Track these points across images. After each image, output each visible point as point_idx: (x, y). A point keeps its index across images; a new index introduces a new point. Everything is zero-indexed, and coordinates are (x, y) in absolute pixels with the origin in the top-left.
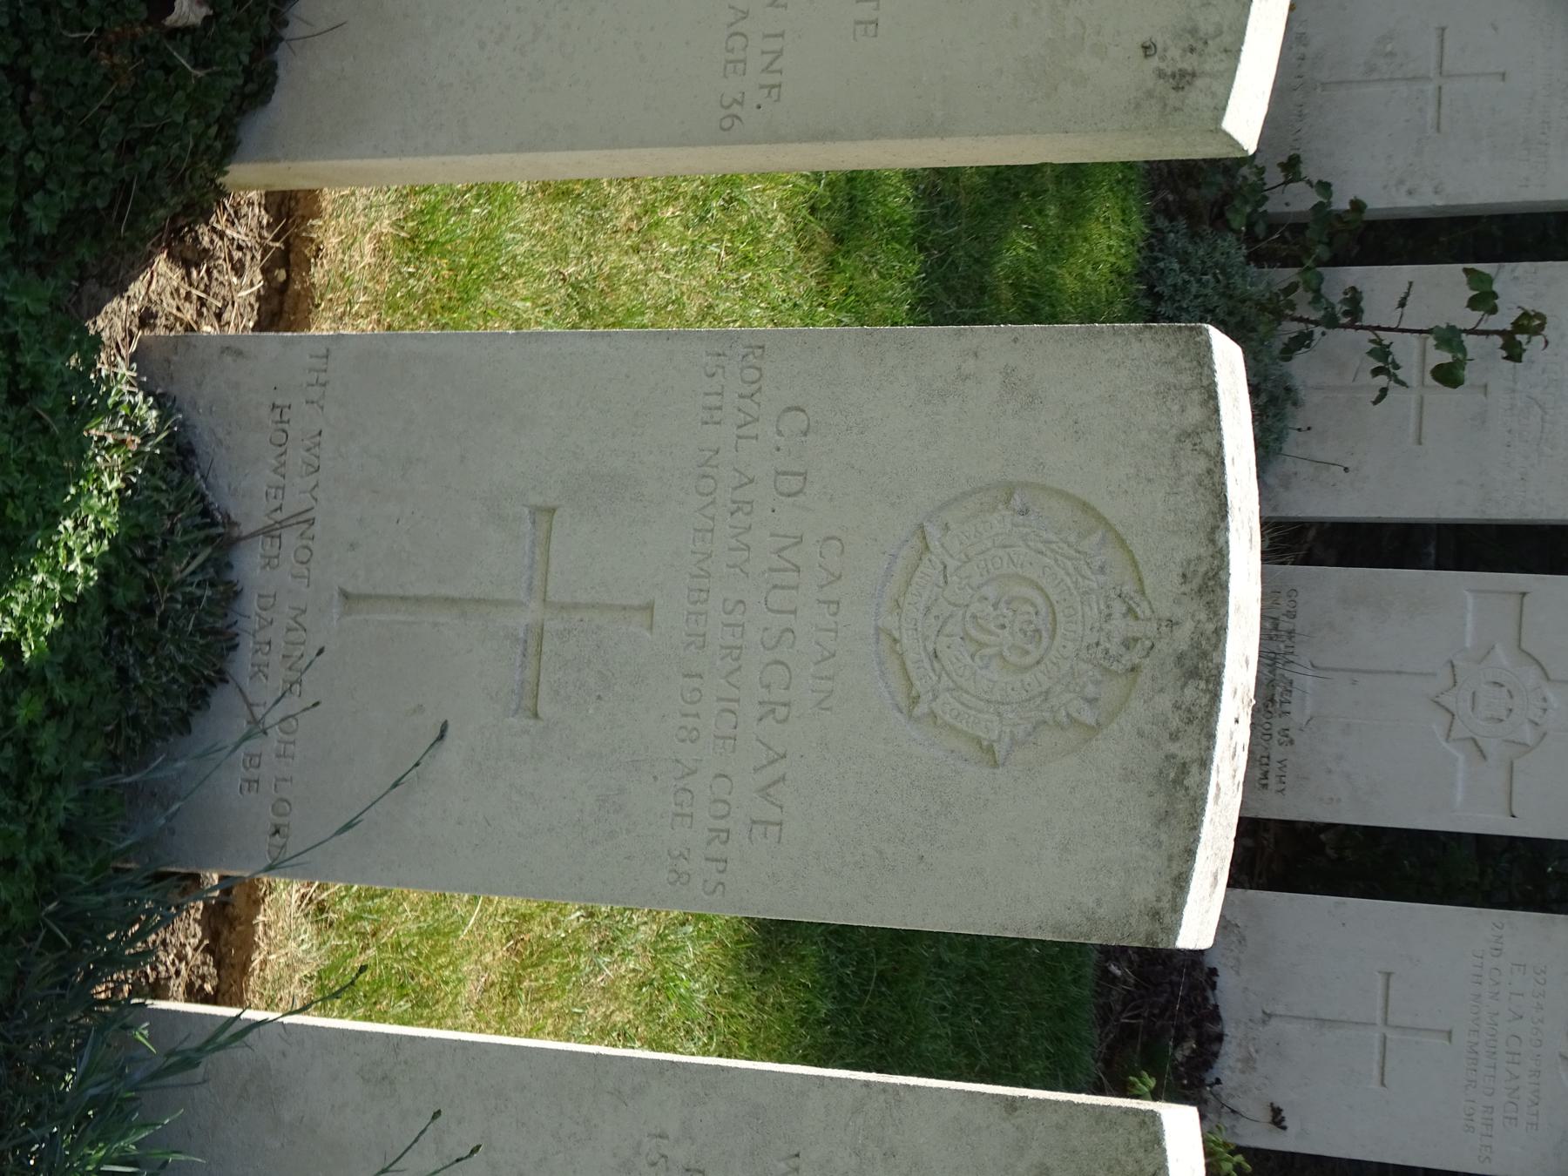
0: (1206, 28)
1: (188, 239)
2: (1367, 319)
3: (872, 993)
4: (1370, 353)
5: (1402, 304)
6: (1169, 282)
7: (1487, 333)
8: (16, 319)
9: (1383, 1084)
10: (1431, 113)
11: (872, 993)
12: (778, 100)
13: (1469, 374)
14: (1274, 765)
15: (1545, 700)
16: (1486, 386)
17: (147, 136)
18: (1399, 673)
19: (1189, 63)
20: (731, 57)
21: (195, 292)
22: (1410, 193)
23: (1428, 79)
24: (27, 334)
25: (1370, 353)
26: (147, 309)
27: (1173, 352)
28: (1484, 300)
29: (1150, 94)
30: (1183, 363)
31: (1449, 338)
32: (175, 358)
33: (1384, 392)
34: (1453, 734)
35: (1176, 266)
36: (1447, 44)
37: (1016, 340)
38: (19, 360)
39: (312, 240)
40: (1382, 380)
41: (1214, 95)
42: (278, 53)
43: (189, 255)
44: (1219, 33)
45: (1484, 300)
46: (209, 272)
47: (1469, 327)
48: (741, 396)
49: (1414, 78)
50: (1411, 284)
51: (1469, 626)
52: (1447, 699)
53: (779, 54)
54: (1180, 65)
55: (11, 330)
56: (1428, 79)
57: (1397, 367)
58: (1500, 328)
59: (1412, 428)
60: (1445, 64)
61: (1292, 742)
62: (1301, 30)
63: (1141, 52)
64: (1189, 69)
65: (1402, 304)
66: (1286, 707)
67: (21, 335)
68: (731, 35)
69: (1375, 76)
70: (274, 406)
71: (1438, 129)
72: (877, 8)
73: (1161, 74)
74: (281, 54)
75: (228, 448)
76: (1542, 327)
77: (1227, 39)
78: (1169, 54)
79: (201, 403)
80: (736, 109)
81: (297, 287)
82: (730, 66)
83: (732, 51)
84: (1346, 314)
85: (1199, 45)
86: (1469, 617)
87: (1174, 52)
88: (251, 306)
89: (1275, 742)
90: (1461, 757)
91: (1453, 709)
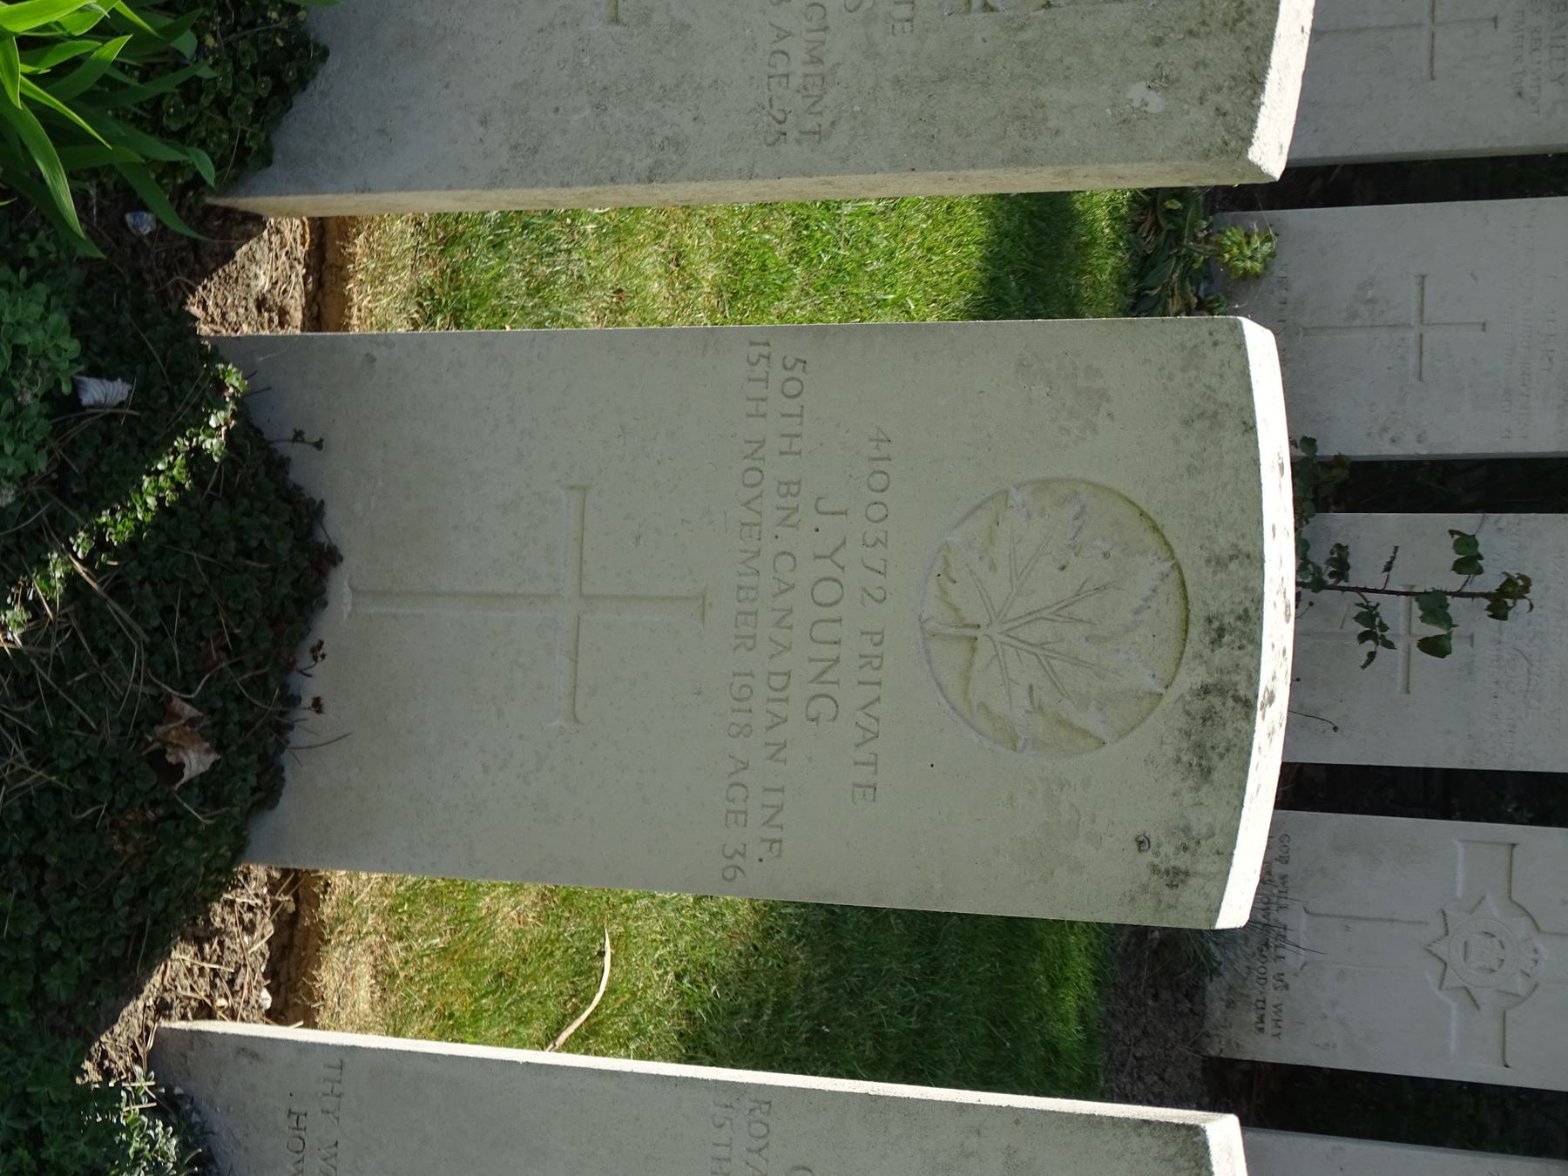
0: (1199, 828)
1: (200, 922)
3: (873, 987)
4: (1357, 618)
5: (1388, 568)
7: (1472, 595)
8: (39, 1110)
9: (1420, 378)
11: (873, 987)
12: (779, 856)
14: (1270, 1009)
15: (1536, 951)
16: (1472, 637)
17: (161, 881)
18: (1392, 920)
19: (1182, 861)
20: (732, 806)
21: (207, 966)
22: (1393, 441)
23: (1410, 326)
24: (50, 1124)
25: (1357, 618)
26: (163, 999)
27: (1172, 1150)
28: (1468, 559)
29: (1144, 889)
30: (1182, 1162)
31: (1434, 605)
32: (191, 1054)
33: (1372, 655)
34: (1447, 983)
36: (1427, 292)
37: (1017, 1122)
38: (43, 1156)
39: (320, 878)
40: (1370, 645)
41: (1207, 896)
42: (292, 476)
43: (201, 934)
44: (1211, 834)
45: (1468, 559)
46: (221, 943)
48: (750, 1150)
49: (1394, 326)
50: (1396, 548)
51: (1460, 876)
52: (1440, 949)
53: (780, 809)
54: (1173, 863)
55: (35, 1122)
56: (1410, 326)
57: (1384, 628)
59: (1400, 677)
60: (1427, 314)
61: (1287, 987)
62: (1282, 273)
63: (1134, 846)
64: (1183, 867)
65: (1388, 568)
66: (1281, 952)
67: (44, 1127)
68: (732, 785)
69: (1357, 322)
70: (290, 1113)
71: (1420, 378)
72: (876, 773)
73: (1155, 870)
74: (286, 757)
75: (246, 1149)
76: (1526, 588)
77: (1219, 841)
78: (1163, 851)
79: (218, 1101)
80: (738, 860)
81: (307, 922)
82: (731, 816)
83: (733, 801)
84: (1332, 575)
85: (1192, 845)
86: (1460, 867)
87: (1167, 849)
88: (262, 955)
89: (1270, 986)
90: (1454, 1006)
91: (1445, 958)
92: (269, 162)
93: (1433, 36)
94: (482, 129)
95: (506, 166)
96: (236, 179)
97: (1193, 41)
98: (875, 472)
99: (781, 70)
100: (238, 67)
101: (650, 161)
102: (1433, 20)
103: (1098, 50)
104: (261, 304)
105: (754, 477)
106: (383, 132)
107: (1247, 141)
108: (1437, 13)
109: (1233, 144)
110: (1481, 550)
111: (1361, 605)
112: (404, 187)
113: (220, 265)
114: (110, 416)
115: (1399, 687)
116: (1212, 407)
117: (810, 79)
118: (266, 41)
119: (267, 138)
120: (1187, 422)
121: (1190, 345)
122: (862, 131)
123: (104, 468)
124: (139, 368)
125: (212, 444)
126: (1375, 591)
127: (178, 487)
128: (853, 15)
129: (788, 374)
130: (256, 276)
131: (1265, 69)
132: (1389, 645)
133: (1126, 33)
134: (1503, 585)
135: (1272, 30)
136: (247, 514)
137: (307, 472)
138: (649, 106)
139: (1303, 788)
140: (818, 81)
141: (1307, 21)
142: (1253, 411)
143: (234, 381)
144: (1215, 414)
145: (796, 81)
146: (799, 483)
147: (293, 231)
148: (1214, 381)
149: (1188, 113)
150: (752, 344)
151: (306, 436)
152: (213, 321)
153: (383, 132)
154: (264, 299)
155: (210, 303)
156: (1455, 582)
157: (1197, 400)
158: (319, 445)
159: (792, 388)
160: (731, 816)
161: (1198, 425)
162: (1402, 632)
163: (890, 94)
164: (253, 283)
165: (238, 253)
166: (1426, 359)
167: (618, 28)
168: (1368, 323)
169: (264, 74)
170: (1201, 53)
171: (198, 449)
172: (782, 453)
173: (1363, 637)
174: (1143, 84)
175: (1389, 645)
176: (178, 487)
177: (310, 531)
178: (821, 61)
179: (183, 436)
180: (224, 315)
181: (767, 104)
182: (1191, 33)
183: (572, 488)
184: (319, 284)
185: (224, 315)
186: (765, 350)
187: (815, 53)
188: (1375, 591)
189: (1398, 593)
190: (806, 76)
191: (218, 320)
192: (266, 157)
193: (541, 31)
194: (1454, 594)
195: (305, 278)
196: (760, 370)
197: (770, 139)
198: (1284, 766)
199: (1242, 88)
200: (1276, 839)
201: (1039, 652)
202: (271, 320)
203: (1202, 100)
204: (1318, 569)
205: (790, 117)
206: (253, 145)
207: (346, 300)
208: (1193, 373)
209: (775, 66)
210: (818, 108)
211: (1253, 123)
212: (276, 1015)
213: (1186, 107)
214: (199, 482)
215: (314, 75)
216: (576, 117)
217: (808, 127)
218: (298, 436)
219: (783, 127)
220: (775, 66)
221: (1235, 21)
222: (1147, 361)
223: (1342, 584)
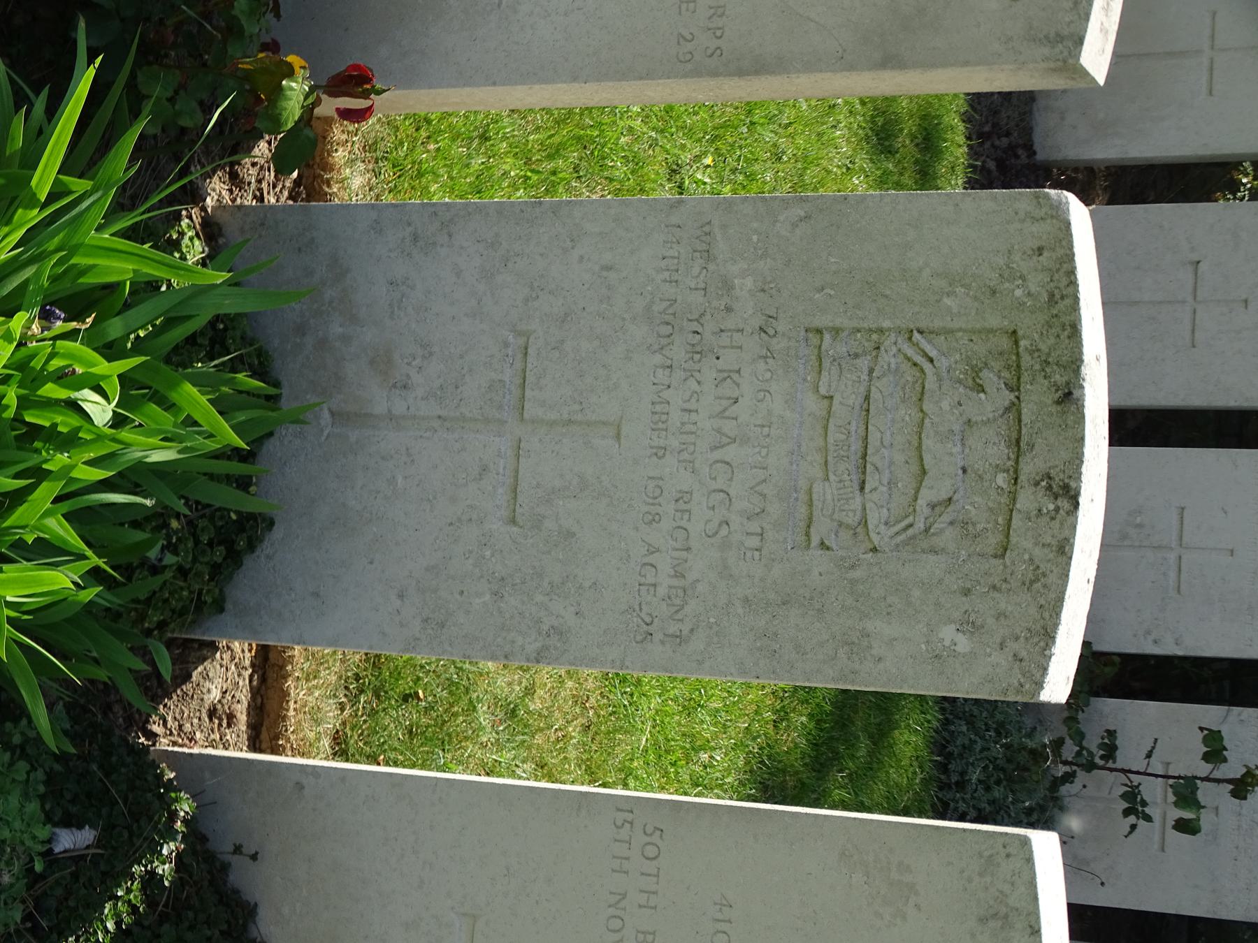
2: (1122, 761)
5: (1149, 756)
6: (958, 743)
9: (1179, 591)
10: (1172, 575)
13: (1206, 820)
16: (1217, 808)
23: (1172, 549)
28: (1215, 750)
33: (1133, 827)
35: (964, 728)
36: (1186, 527)
40: (1132, 819)
42: (231, 878)
45: (1215, 750)
47: (1203, 775)
49: (1159, 547)
57: (1144, 803)
58: (1231, 776)
60: (1185, 539)
65: (1149, 756)
71: (1179, 591)
84: (1102, 757)
92: (221, 610)
93: (1195, 312)
94: (399, 602)
95: (418, 635)
96: (193, 622)
97: (996, 595)
98: (718, 932)
99: (650, 580)
100: (197, 542)
101: (538, 645)
103: (916, 593)
104: (212, 713)
105: (616, 924)
106: (316, 595)
108: (1198, 293)
109: (1027, 686)
110: (1226, 743)
111: (1126, 785)
113: (179, 686)
114: (76, 858)
115: (1156, 846)
116: (1004, 910)
117: (674, 591)
118: (222, 518)
119: (221, 590)
120: (983, 920)
121: (986, 854)
122: (715, 639)
123: (72, 903)
124: (104, 811)
125: (165, 869)
126: (1138, 773)
127: (134, 909)
128: (712, 540)
129: (648, 839)
130: (209, 691)
131: (1056, 625)
132: (1148, 818)
133: (940, 581)
134: (1243, 776)
135: (1063, 592)
136: (191, 928)
137: (242, 876)
138: (539, 598)
140: (681, 593)
141: (1092, 574)
142: (1038, 918)
143: (185, 807)
144: (1006, 917)
145: (662, 591)
146: (654, 933)
147: (242, 649)
148: (1006, 888)
149: (990, 655)
150: (619, 810)
151: (244, 850)
152: (171, 733)
153: (316, 595)
154: (215, 709)
155: (169, 719)
156: (1204, 769)
157: (991, 903)
158: (254, 857)
159: (651, 851)
161: (992, 924)
162: (1159, 801)
163: (740, 611)
164: (205, 697)
165: (195, 674)
167: (515, 529)
168: (1137, 544)
169: (220, 544)
170: (1003, 605)
171: (152, 873)
172: (640, 906)
173: (1126, 813)
174: (953, 627)
175: (1148, 818)
176: (134, 909)
177: (245, 928)
178: (684, 577)
179: (139, 863)
180: (180, 726)
181: (637, 608)
182: (994, 587)
183: (464, 915)
184: (263, 680)
185: (180, 726)
186: (629, 817)
187: (679, 569)
188: (1138, 773)
189: (1157, 776)
190: (670, 587)
191: (175, 732)
192: (219, 606)
193: (451, 524)
194: (1203, 779)
195: (251, 677)
196: (624, 833)
197: (639, 638)
199: (1036, 640)
200: (1052, 578)
202: (220, 725)
203: (1002, 646)
204: (1091, 754)
205: (656, 620)
206: (209, 599)
207: (285, 695)
208: (988, 879)
209: (645, 576)
210: (679, 616)
211: (1045, 670)
212: (254, 746)
213: (988, 650)
214: (150, 902)
215: (262, 541)
216: (477, 601)
217: (671, 631)
218: (238, 849)
219: (651, 629)
220: (645, 576)
221: (1032, 582)
222: (950, 863)
223: (1110, 765)
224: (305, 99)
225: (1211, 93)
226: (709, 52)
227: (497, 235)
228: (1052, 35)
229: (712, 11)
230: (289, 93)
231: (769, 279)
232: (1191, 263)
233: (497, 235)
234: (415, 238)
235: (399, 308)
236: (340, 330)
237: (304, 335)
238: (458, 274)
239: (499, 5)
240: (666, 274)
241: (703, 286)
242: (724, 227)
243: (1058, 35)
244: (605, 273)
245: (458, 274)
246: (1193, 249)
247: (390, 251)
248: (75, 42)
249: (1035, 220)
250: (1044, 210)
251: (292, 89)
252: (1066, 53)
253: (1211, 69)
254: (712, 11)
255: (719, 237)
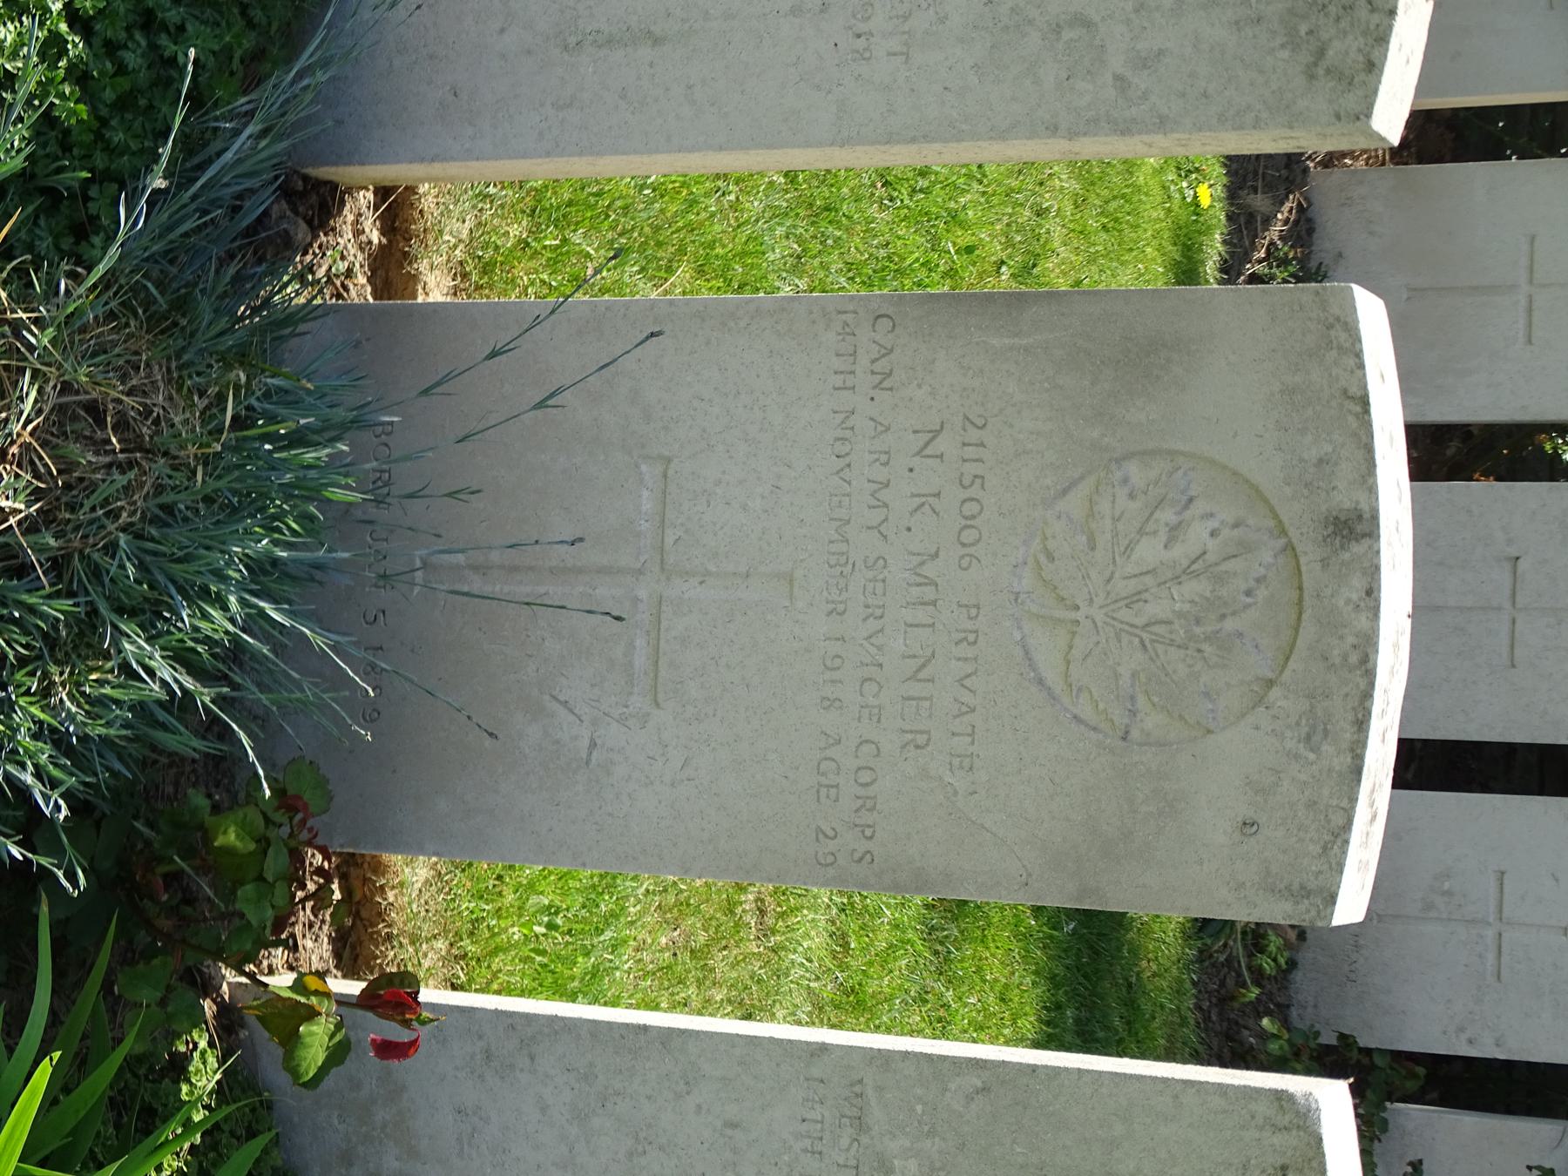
10: (1491, 957)
22: (1470, 1042)
23: (1489, 924)
36: (1506, 896)
60: (1506, 912)
69: (1433, 914)
72: (973, 743)
83: (824, 774)
93: (1514, 622)
102: (1514, 603)
107: (1369, 115)
108: (1518, 598)
112: (469, 155)
139: (1426, 765)
160: (824, 791)
166: (1505, 959)
168: (1444, 916)
198: (1400, 740)
201: (1144, 635)
224: (331, 1038)
225: (1529, 342)
226: (857, 856)
227: (591, 1065)
228: (1296, 887)
229: (860, 802)
230: (308, 1040)
231: (938, 1165)
232: (1508, 559)
233: (591, 1065)
234: (488, 1055)
235: (470, 1144)
236: (396, 1164)
237: (351, 1165)
238: (544, 1109)
239: (587, 763)
240: (807, 1143)
241: (854, 1163)
242: (880, 1089)
243: (1302, 887)
244: (729, 1132)
245: (544, 1109)
246: (1510, 542)
247: (457, 1068)
248: (36, 918)
249: (1277, 1129)
250: (1287, 1117)
251: (312, 1034)
252: (1313, 913)
253: (1530, 311)
254: (860, 802)
255: (873, 1103)
